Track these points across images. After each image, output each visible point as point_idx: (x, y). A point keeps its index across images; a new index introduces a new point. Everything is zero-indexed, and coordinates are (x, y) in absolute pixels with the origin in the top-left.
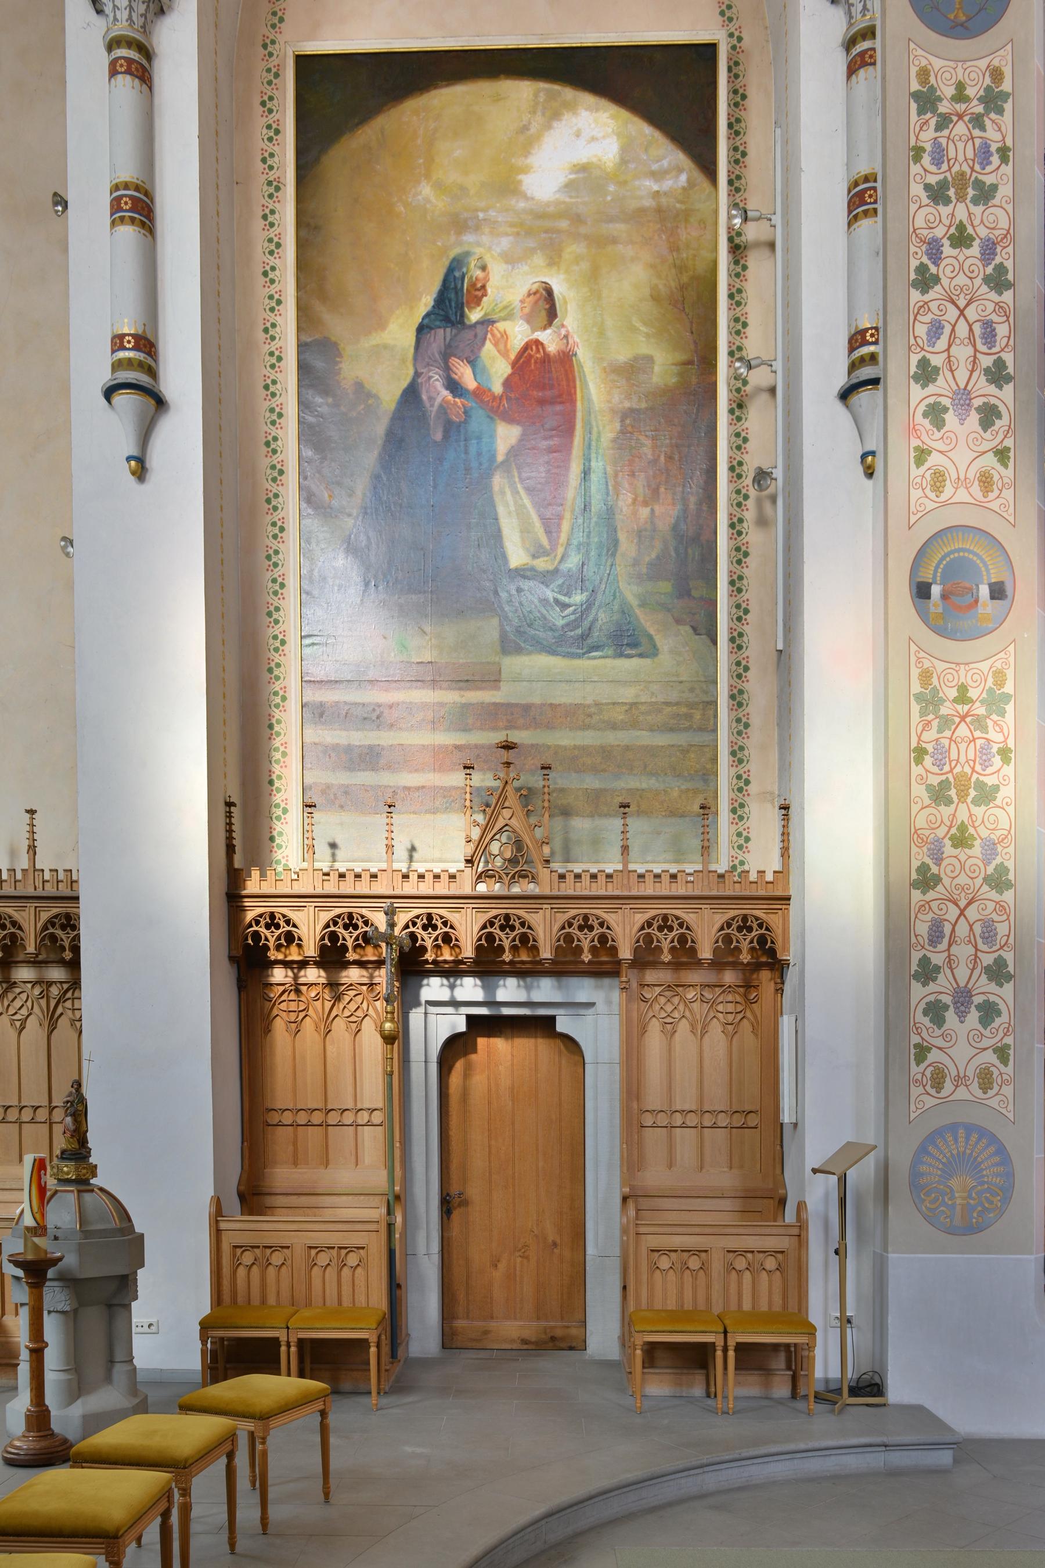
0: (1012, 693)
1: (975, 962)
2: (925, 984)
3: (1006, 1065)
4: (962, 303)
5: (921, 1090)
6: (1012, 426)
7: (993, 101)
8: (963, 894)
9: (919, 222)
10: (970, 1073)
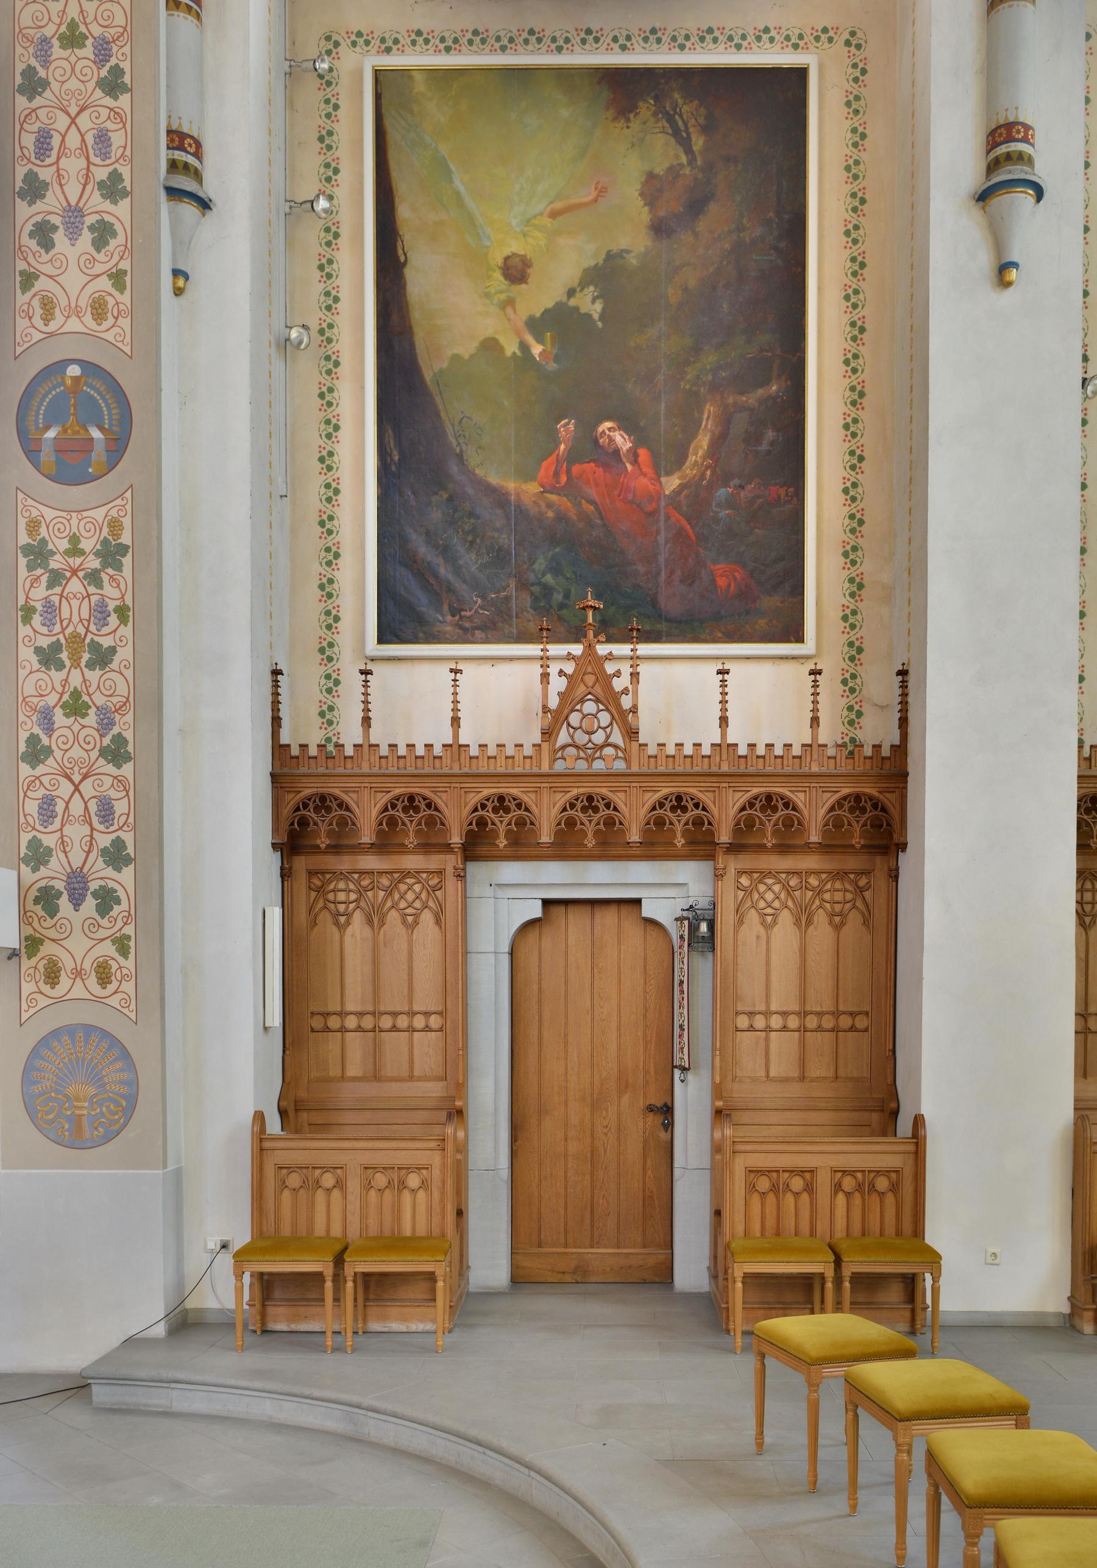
0: (130, 544)
1: (91, 844)
2: (31, 203)
3: (126, 957)
4: (73, 110)
5: (26, 322)
6: (129, 245)
7: (112, 554)
8: (76, 769)
9: (29, 689)
10: (87, 965)
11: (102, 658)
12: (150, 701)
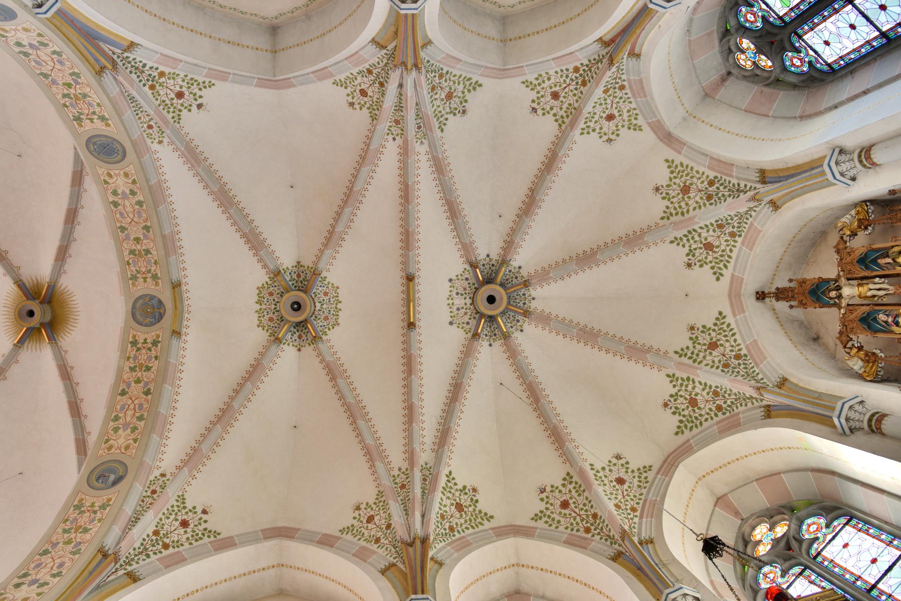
11: (148, 369)
12: (119, 244)
